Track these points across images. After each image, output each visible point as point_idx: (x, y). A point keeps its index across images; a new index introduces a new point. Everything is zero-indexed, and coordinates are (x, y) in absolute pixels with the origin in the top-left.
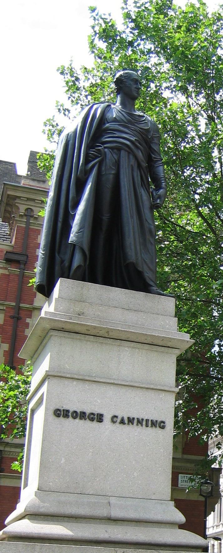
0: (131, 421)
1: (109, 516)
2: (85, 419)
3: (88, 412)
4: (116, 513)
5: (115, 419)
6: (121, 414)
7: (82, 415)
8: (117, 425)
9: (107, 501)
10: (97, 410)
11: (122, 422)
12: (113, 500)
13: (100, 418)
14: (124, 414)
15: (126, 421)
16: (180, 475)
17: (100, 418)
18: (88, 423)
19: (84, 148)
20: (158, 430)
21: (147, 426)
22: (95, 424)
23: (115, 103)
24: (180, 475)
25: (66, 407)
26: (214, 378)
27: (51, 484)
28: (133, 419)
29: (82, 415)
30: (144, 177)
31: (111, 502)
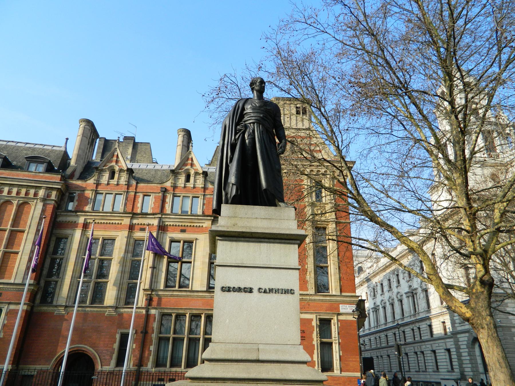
0: (271, 290)
1: (258, 359)
2: (242, 292)
3: (242, 287)
4: (262, 357)
5: (261, 290)
6: (264, 287)
7: (239, 290)
8: (262, 294)
9: (257, 348)
10: (248, 286)
11: (265, 292)
12: (261, 347)
13: (251, 291)
14: (266, 286)
15: (268, 291)
16: (340, 305)
17: (251, 291)
18: (243, 294)
19: (13, 348)
20: (290, 295)
21: (282, 293)
22: (248, 294)
23: (164, 189)
24: (340, 305)
25: (228, 285)
26: (437, 182)
27: (220, 337)
28: (273, 289)
29: (239, 290)
30: (271, 138)
31: (260, 348)
